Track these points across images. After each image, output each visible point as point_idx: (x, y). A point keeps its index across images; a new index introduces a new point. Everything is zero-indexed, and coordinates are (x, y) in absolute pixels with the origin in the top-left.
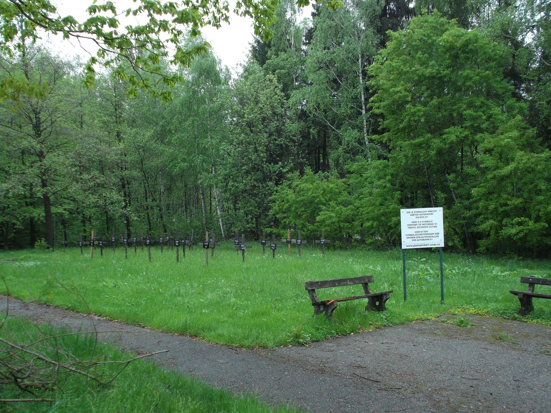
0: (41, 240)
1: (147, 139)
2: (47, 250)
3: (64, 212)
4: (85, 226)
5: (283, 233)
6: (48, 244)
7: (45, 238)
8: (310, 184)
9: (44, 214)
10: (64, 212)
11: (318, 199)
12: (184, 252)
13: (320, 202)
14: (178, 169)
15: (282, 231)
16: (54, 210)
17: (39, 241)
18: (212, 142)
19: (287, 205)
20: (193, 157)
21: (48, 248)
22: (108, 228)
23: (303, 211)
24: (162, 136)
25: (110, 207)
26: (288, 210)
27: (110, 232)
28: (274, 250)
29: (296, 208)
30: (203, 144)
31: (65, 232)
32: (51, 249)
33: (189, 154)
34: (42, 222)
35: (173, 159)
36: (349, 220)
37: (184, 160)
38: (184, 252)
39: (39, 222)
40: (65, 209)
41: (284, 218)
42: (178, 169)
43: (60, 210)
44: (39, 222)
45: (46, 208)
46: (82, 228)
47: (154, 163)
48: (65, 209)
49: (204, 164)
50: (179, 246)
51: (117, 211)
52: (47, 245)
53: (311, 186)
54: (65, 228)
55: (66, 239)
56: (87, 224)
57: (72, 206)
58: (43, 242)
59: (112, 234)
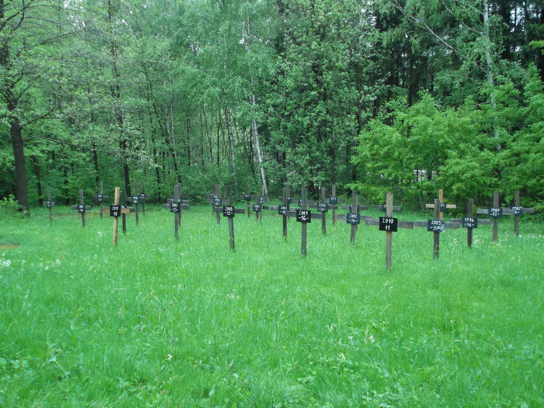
0: (8, 197)
2: (18, 214)
3: (41, 155)
5: (375, 191)
6: (19, 203)
7: (15, 195)
8: (428, 118)
9: (13, 158)
10: (41, 155)
13: (446, 146)
15: (373, 188)
16: (27, 152)
17: (5, 198)
18: (257, 58)
21: (20, 210)
23: (410, 158)
24: (179, 47)
26: (388, 155)
28: (470, 229)
31: (39, 184)
32: (25, 212)
33: (221, 75)
34: (9, 170)
36: (497, 171)
37: (214, 84)
39: (5, 170)
40: (43, 151)
41: (380, 168)
43: (37, 152)
44: (5, 170)
45: (15, 147)
46: (63, 180)
48: (43, 151)
52: (18, 206)
53: (429, 119)
55: (40, 194)
57: (53, 147)
58: (11, 201)
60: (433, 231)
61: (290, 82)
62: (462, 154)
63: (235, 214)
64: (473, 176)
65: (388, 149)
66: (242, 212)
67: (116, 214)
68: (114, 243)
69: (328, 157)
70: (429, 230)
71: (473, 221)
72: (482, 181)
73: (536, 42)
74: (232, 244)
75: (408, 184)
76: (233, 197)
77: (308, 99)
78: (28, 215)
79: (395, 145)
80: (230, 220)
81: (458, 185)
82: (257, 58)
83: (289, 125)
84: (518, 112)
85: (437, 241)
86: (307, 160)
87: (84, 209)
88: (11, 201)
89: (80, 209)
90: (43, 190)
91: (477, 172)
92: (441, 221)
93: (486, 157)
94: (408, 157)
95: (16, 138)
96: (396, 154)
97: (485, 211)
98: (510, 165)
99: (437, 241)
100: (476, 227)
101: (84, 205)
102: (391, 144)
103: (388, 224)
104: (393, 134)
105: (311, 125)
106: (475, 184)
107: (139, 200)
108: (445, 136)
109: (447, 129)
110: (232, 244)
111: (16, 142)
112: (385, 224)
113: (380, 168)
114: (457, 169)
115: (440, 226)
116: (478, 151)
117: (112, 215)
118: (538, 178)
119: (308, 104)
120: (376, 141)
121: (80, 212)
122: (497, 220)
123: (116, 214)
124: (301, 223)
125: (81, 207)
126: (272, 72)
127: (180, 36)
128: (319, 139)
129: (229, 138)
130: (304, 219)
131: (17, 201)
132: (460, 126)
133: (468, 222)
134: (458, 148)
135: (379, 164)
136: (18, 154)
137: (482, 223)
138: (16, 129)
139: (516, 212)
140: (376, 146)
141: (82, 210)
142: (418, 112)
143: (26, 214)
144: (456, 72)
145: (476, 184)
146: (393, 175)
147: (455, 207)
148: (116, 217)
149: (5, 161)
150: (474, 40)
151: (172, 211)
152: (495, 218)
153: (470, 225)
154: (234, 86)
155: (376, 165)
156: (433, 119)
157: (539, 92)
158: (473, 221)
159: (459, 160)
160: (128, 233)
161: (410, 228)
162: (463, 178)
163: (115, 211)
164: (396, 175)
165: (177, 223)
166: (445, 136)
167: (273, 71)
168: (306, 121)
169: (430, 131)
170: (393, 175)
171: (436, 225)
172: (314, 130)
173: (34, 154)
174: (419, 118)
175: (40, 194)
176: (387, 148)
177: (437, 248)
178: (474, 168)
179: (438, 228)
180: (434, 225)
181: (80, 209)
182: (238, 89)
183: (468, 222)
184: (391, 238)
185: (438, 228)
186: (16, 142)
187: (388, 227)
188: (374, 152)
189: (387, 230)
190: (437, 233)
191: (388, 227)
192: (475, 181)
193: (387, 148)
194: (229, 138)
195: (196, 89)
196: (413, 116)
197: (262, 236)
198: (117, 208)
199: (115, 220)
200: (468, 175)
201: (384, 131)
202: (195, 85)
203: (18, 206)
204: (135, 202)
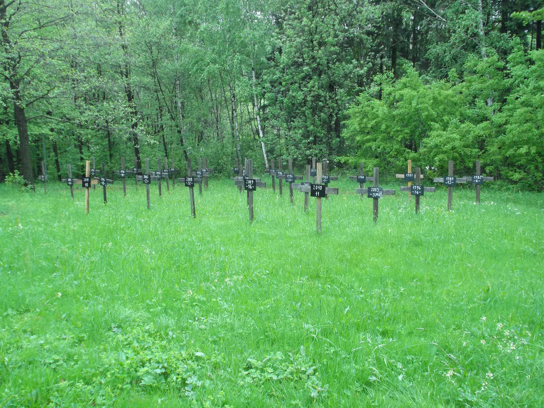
0: (14, 173)
1: (161, 32)
2: (23, 188)
3: (50, 133)
4: (81, 153)
5: (365, 163)
6: (24, 178)
8: (415, 90)
11: (426, 113)
12: (292, 195)
14: (205, 73)
15: (363, 161)
17: (11, 174)
19: (373, 123)
20: (226, 57)
21: (26, 185)
22: (111, 156)
23: (397, 131)
25: (113, 126)
26: (375, 129)
27: (113, 161)
29: (387, 127)
30: (240, 37)
31: (57, 161)
32: (29, 186)
35: (198, 60)
36: (481, 143)
37: (214, 62)
38: (292, 195)
40: (52, 130)
41: (368, 141)
42: (205, 73)
46: (78, 156)
47: (167, 66)
49: (243, 66)
50: (149, 183)
51: (122, 131)
52: (23, 181)
53: (414, 93)
54: (56, 155)
55: (59, 170)
56: (84, 149)
58: (16, 175)
59: (114, 164)
60: (372, 197)
61: (284, 59)
62: (445, 127)
63: (195, 184)
64: (453, 148)
65: (376, 122)
66: (264, 185)
67: (87, 185)
68: (86, 211)
69: (323, 131)
70: (369, 196)
71: (420, 189)
72: (462, 153)
73: (518, 13)
74: (194, 212)
75: (396, 157)
76: (241, 169)
77: (303, 74)
78: (33, 189)
79: (383, 119)
80: (191, 189)
81: (441, 156)
82: (254, 35)
83: (285, 100)
84: (402, 92)
85: (376, 207)
86: (300, 134)
87: (72, 182)
88: (16, 175)
89: (68, 182)
90: (61, 167)
91: (457, 144)
92: (379, 188)
93: (467, 128)
94: (395, 129)
95: (20, 119)
96: (383, 127)
97: (441, 180)
98: (490, 136)
99: (376, 207)
100: (422, 194)
101: (72, 179)
102: (377, 116)
103: (318, 190)
104: (380, 108)
105: (305, 101)
106: (456, 155)
107: (125, 173)
108: (430, 108)
109: (431, 101)
110: (194, 212)
111: (20, 121)
112: (316, 191)
113: (368, 141)
114: (438, 140)
115: (379, 193)
116: (459, 123)
117: (84, 186)
118: (515, 148)
119: (303, 79)
120: (365, 115)
121: (68, 185)
122: (451, 188)
123: (87, 185)
124: (188, 188)
125: (70, 180)
126: (269, 49)
127: (183, 14)
128: (314, 113)
129: (233, 114)
130: (251, 187)
131: (22, 176)
132: (445, 98)
133: (416, 190)
134: (442, 120)
135: (368, 137)
136: (23, 134)
137: (428, 191)
138: (19, 111)
139: (477, 181)
140: (365, 120)
141: (70, 183)
142: (405, 86)
143: (31, 188)
144: (447, 44)
145: (457, 155)
146: (381, 147)
147: (397, 175)
148: (88, 188)
149: (16, 139)
150: (463, 13)
151: (144, 182)
152: (450, 186)
153: (418, 193)
154: (233, 63)
155: (365, 138)
156: (418, 92)
157: (521, 63)
158: (420, 189)
159: (442, 132)
160: (109, 203)
161: (335, 194)
162: (444, 149)
163: (86, 182)
164: (384, 147)
165: (250, 201)
166: (430, 108)
167: (269, 48)
168: (300, 96)
169: (414, 104)
170: (381, 147)
171: (375, 192)
172: (309, 104)
173: (43, 132)
174: (405, 91)
175: (59, 170)
176: (375, 121)
177: (376, 213)
178: (454, 140)
179: (377, 194)
180: (373, 192)
181: (68, 182)
182: (236, 66)
183: (416, 190)
184: (321, 204)
185: (377, 194)
186: (20, 121)
187: (317, 193)
188: (362, 126)
189: (317, 196)
190: (376, 199)
191: (317, 193)
192: (457, 152)
193: (375, 121)
194: (233, 114)
195: (198, 66)
196: (400, 90)
197: (281, 209)
198: (88, 179)
199: (86, 190)
200: (449, 146)
201: (373, 105)
202: (197, 62)
203: (23, 181)
204: (123, 175)
